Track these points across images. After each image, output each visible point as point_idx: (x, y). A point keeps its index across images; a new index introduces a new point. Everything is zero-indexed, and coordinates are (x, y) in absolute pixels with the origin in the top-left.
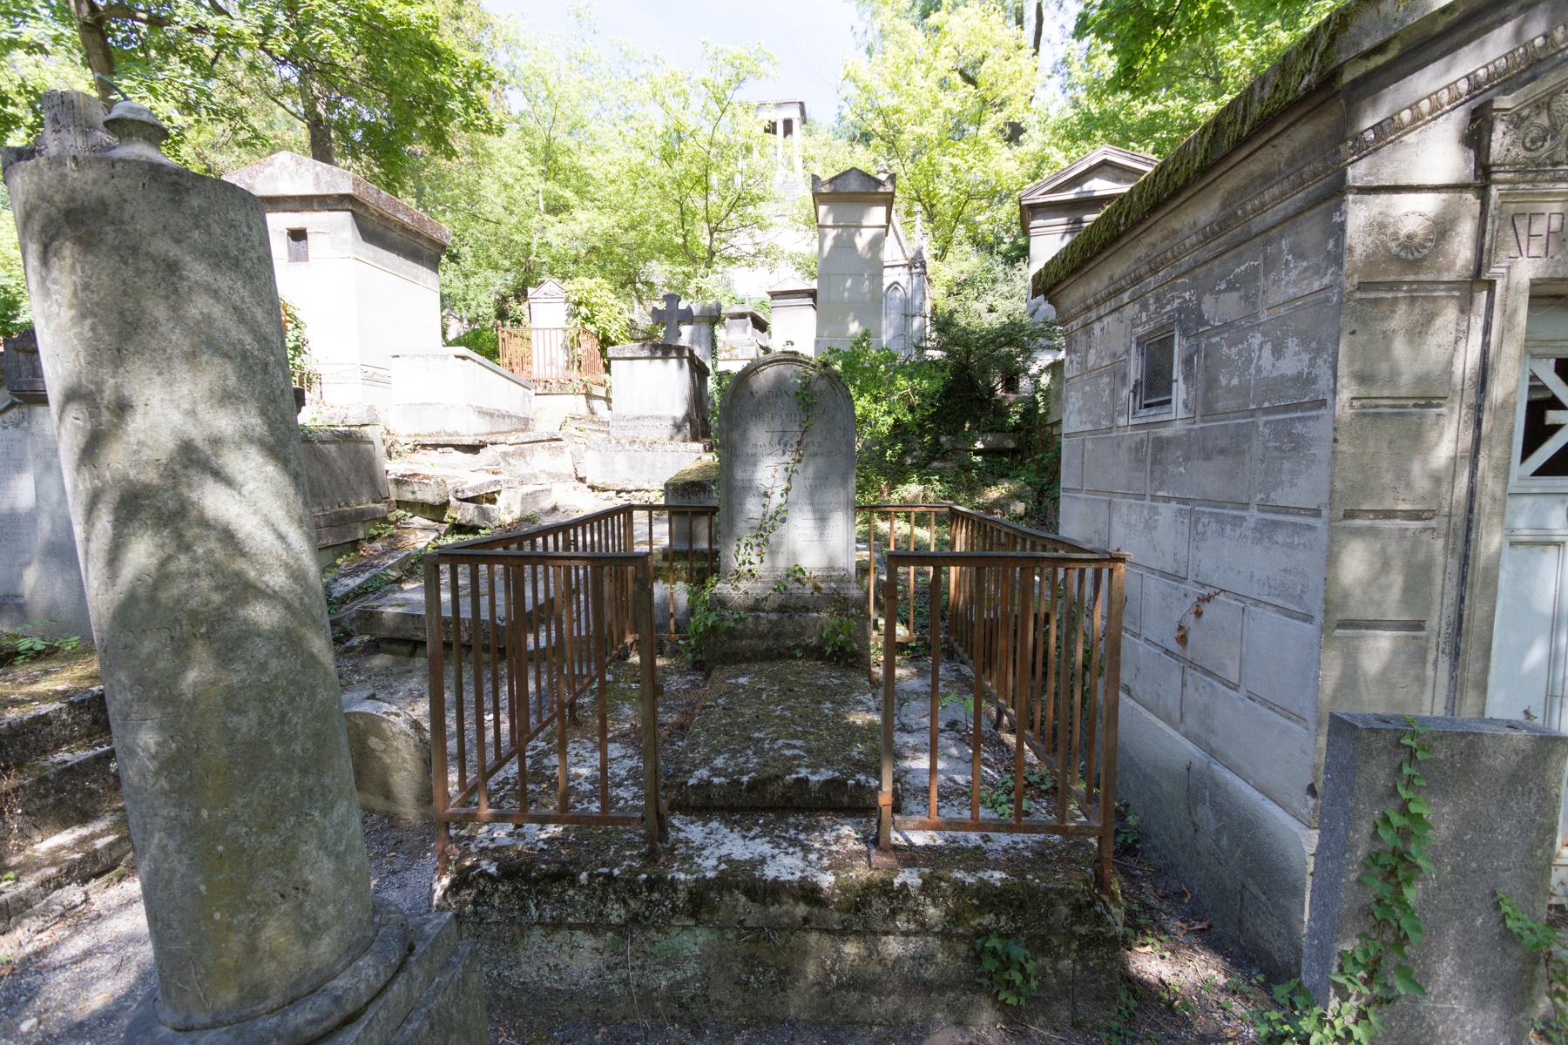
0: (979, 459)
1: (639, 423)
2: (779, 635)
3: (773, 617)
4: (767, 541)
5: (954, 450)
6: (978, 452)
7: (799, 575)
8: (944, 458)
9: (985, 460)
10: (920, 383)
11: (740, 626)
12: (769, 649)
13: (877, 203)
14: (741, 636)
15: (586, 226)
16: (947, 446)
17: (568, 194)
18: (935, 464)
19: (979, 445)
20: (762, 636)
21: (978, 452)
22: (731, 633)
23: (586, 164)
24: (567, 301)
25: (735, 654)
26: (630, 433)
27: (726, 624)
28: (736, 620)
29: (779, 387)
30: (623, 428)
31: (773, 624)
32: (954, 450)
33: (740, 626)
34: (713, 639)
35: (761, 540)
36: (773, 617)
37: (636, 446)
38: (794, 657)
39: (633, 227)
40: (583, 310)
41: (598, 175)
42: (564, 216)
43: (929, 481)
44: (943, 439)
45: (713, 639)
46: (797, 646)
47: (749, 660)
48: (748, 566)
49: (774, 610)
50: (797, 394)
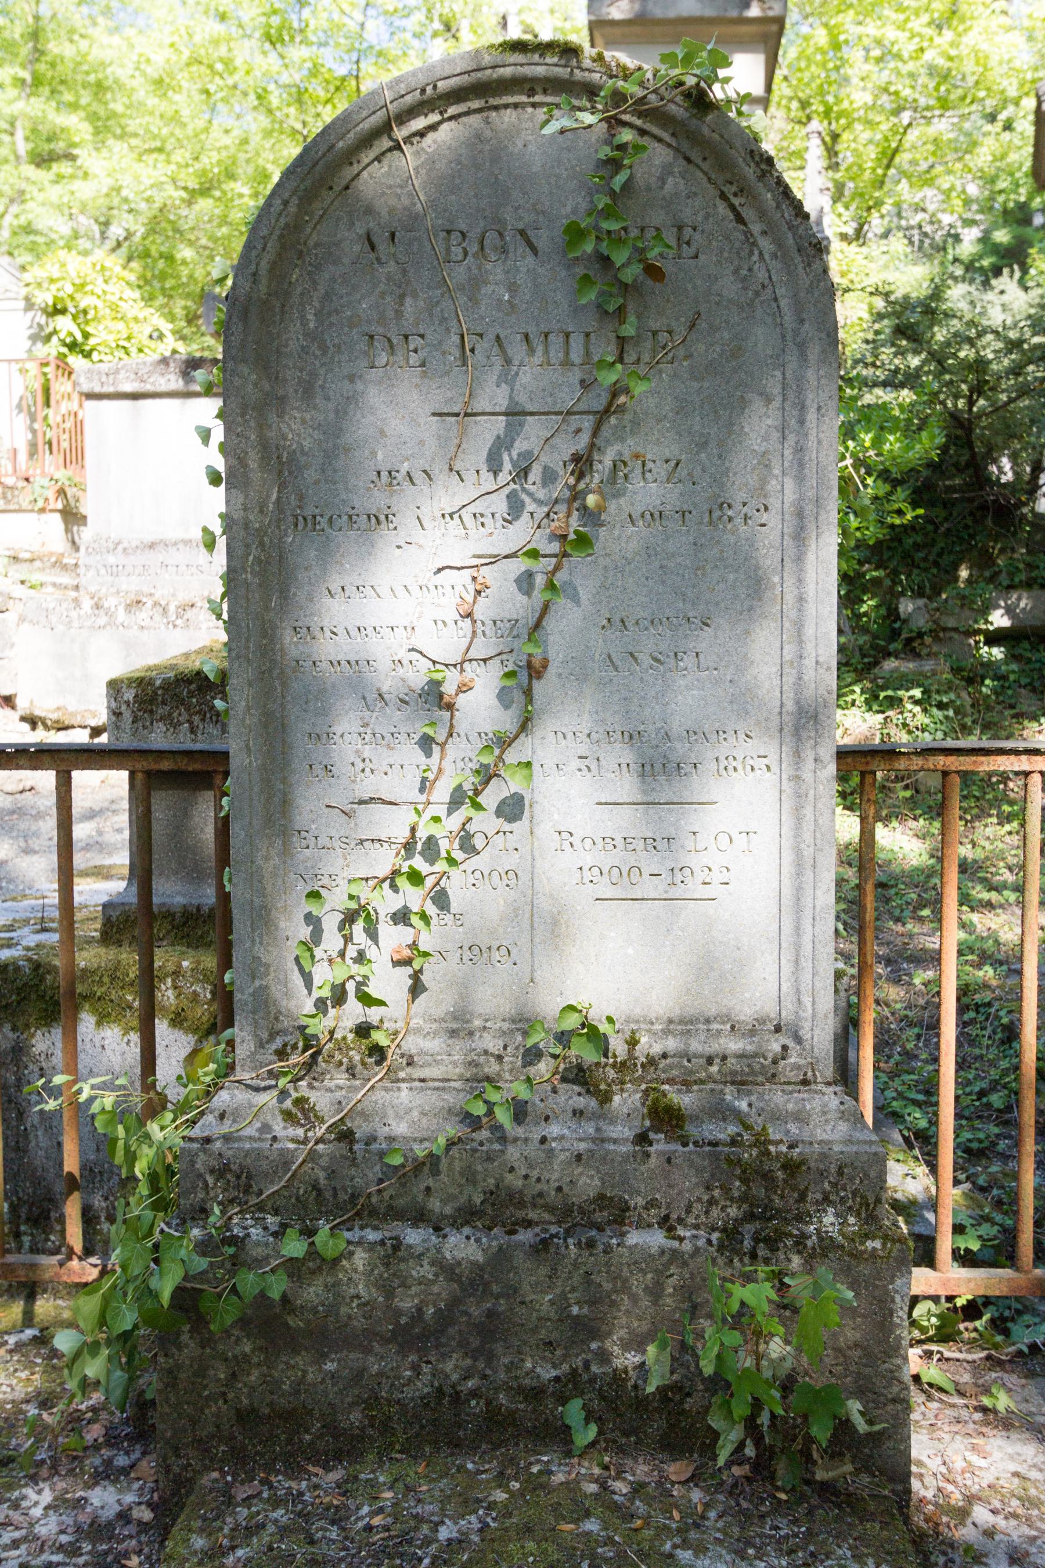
0: (998, 653)
1: (155, 558)
2: (491, 1330)
3: (462, 1247)
4: (441, 899)
5: (938, 632)
6: (994, 638)
7: (583, 1052)
8: (911, 649)
9: (1012, 657)
10: (877, 442)
11: (313, 1293)
12: (448, 1397)
13: (744, 44)
14: (324, 1335)
15: (106, 183)
16: (921, 622)
17: (76, 125)
18: (890, 664)
19: (999, 620)
20: (415, 1336)
21: (994, 638)
22: (269, 1322)
23: (107, 55)
24: (29, 305)
25: (292, 1418)
26: (132, 585)
27: (248, 1282)
28: (293, 1267)
29: (484, 191)
30: (114, 571)
31: (473, 1281)
32: (938, 632)
33: (313, 1293)
34: (190, 1347)
35: (413, 897)
36: (462, 1247)
37: (143, 616)
38: (559, 1436)
39: (205, 191)
40: (65, 325)
41: (121, 72)
42: (63, 168)
43: (894, 702)
44: (907, 606)
45: (190, 1347)
46: (571, 1384)
47: (344, 1448)
48: (353, 1012)
49: (467, 1216)
50: (575, 234)
